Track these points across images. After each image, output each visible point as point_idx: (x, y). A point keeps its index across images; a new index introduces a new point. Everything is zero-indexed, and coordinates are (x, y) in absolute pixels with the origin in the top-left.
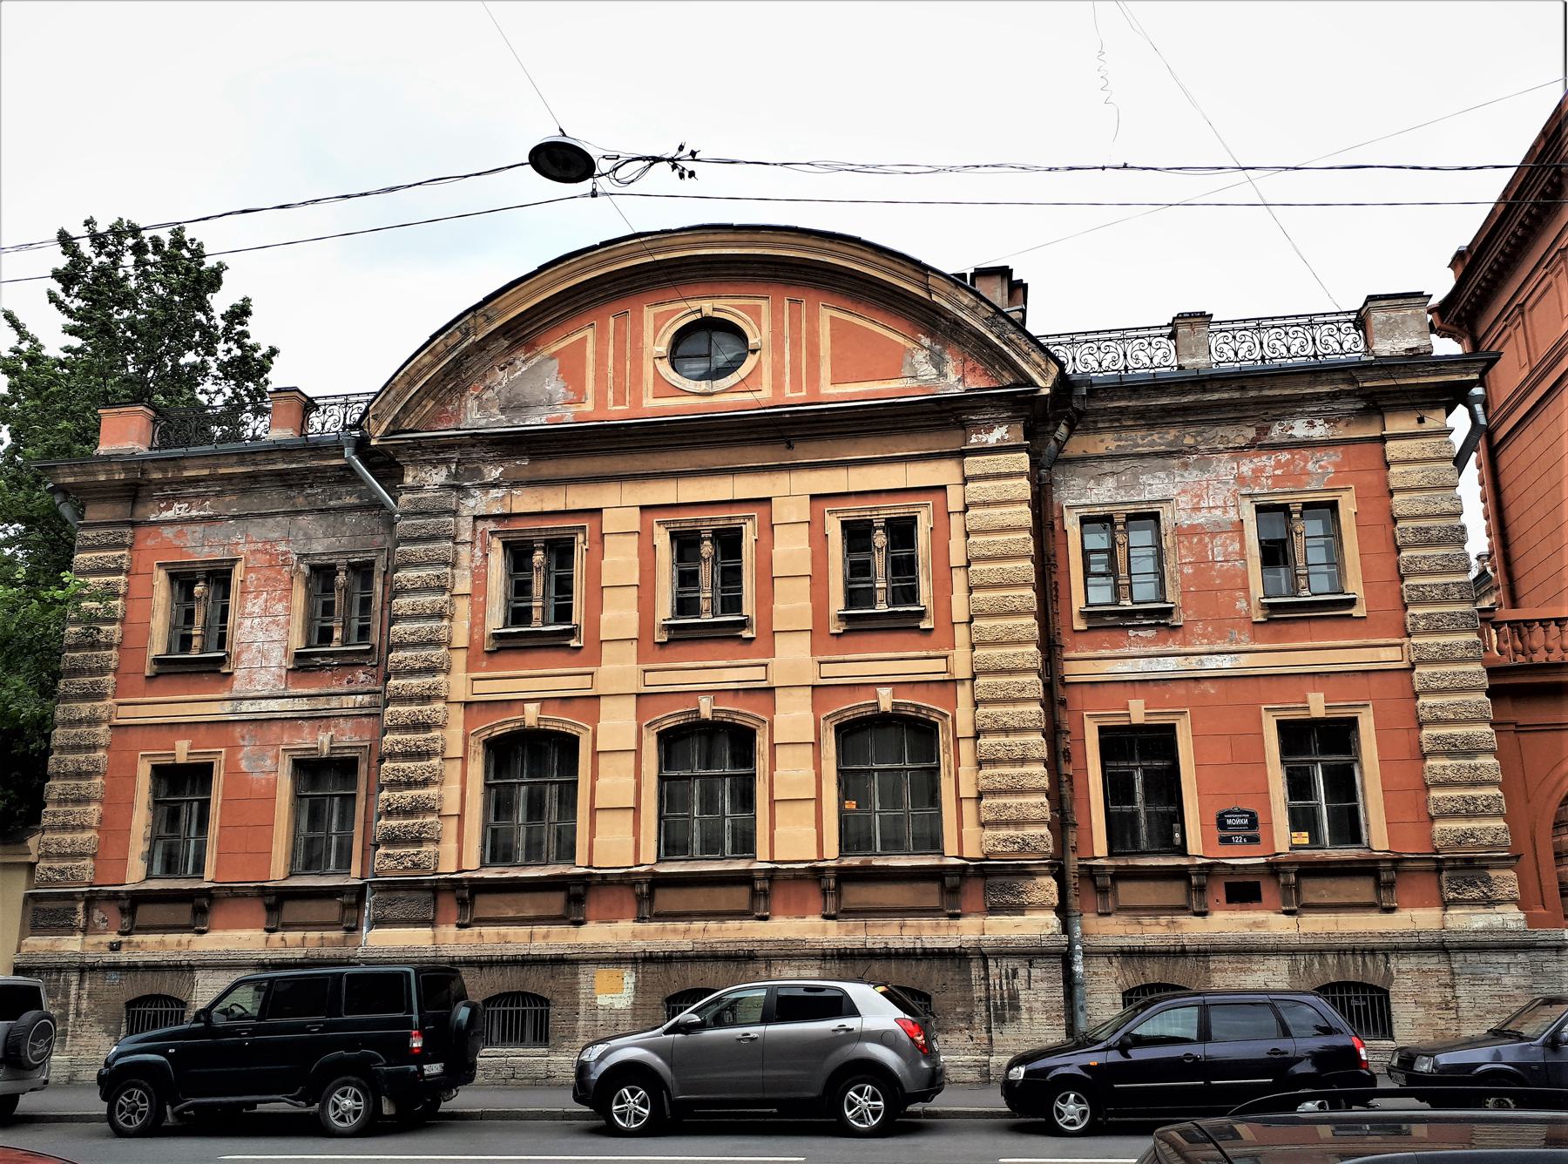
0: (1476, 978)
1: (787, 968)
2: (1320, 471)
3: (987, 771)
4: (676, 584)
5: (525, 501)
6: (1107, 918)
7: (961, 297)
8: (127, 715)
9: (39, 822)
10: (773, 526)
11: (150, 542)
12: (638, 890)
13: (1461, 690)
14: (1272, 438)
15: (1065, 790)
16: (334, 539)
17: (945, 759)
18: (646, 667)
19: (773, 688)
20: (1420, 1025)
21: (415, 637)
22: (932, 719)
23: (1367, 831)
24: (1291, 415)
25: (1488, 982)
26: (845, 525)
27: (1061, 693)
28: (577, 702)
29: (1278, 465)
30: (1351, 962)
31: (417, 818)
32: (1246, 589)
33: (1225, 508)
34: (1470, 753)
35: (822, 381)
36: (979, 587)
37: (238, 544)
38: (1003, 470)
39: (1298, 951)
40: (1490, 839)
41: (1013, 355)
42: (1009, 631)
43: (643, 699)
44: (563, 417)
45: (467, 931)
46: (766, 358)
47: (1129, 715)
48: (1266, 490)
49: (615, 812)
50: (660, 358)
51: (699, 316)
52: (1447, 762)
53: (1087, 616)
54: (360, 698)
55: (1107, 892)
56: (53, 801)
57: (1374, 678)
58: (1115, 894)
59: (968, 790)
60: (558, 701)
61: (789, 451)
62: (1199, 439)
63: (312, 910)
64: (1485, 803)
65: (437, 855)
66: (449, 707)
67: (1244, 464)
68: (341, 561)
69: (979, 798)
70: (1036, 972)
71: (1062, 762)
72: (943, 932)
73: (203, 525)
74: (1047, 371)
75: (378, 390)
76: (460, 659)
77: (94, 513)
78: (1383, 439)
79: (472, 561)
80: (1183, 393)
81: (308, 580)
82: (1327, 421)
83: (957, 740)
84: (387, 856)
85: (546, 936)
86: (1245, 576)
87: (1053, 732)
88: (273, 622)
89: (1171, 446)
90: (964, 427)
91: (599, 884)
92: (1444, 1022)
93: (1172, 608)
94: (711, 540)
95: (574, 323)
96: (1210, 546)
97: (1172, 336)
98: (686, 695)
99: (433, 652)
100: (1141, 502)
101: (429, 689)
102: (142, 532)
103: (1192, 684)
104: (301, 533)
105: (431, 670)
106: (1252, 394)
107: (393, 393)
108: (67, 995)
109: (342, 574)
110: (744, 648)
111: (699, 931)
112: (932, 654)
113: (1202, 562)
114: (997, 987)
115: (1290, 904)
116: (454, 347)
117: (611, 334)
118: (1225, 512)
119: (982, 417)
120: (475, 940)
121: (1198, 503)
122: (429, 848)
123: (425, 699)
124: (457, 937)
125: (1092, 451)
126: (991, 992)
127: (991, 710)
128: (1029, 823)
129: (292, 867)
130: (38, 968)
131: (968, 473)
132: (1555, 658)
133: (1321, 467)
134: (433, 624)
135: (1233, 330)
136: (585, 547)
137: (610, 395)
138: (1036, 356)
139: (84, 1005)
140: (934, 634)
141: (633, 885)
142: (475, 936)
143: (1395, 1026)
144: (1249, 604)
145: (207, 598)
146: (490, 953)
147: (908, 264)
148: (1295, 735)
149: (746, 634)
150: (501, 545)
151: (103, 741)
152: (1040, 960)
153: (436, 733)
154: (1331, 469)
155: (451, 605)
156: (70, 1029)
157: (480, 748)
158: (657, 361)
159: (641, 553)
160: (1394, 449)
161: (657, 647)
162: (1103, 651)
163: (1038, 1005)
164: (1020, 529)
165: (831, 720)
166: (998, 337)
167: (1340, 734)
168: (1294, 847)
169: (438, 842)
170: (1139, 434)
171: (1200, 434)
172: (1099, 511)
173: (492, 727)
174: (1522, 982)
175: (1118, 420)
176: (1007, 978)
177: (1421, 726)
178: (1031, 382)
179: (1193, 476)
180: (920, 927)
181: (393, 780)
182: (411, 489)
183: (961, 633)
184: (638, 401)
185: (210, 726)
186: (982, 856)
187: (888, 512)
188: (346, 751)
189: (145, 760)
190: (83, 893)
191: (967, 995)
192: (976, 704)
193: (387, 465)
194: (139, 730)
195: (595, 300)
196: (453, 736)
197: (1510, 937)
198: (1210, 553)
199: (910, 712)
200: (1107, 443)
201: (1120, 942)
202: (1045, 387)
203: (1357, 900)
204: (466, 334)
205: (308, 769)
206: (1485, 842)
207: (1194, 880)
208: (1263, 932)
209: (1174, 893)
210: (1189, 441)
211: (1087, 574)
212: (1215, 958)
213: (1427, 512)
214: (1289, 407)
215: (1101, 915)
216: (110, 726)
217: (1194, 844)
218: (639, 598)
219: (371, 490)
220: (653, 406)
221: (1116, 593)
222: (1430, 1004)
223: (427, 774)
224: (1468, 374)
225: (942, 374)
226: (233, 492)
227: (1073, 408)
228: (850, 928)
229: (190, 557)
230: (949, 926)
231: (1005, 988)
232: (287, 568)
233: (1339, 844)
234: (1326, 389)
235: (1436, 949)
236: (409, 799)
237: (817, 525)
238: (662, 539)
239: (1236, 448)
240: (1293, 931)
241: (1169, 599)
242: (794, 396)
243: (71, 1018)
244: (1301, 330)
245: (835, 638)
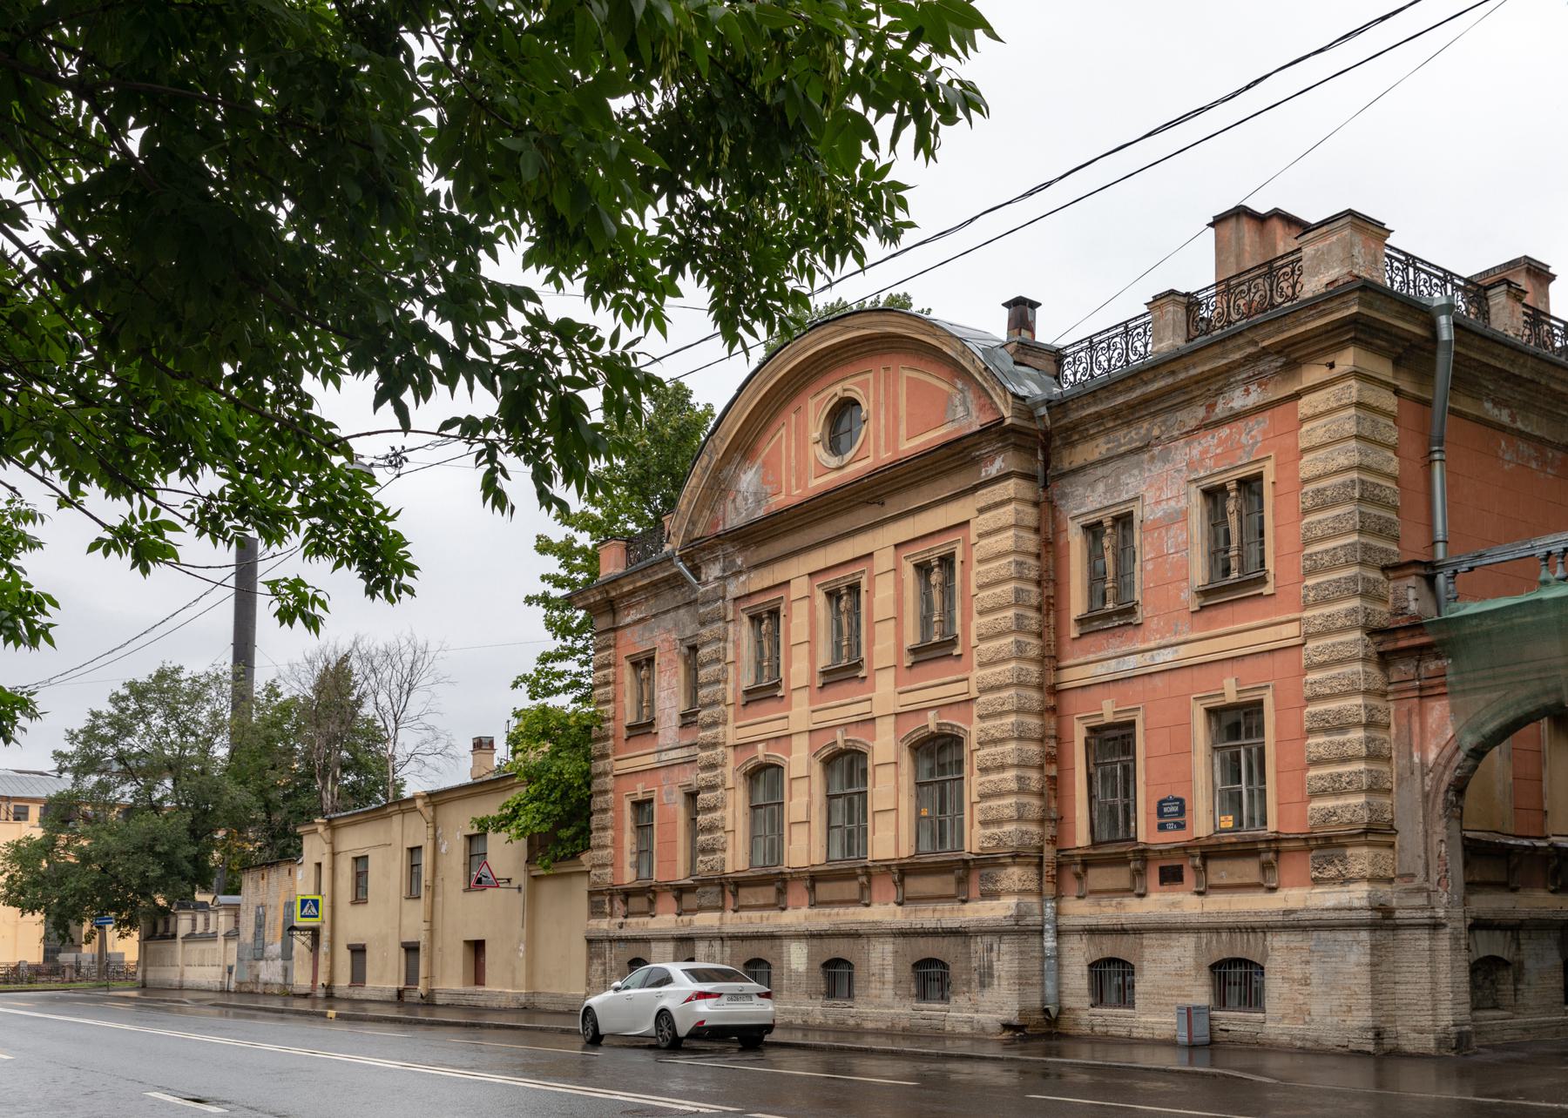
34: (1343, 728)
38: (998, 499)
43: (900, 717)
47: (1223, 694)
51: (836, 399)
57: (1279, 656)
90: (976, 462)
92: (1301, 997)
102: (619, 633)
103: (1146, 679)
106: (1182, 376)
116: (707, 467)
122: (719, 855)
133: (1252, 437)
151: (609, 787)
175: (1102, 424)
179: (1158, 468)
201: (1083, 921)
203: (1247, 880)
208: (1176, 911)
210: (1156, 432)
222: (1294, 980)
224: (1348, 308)
230: (958, 910)
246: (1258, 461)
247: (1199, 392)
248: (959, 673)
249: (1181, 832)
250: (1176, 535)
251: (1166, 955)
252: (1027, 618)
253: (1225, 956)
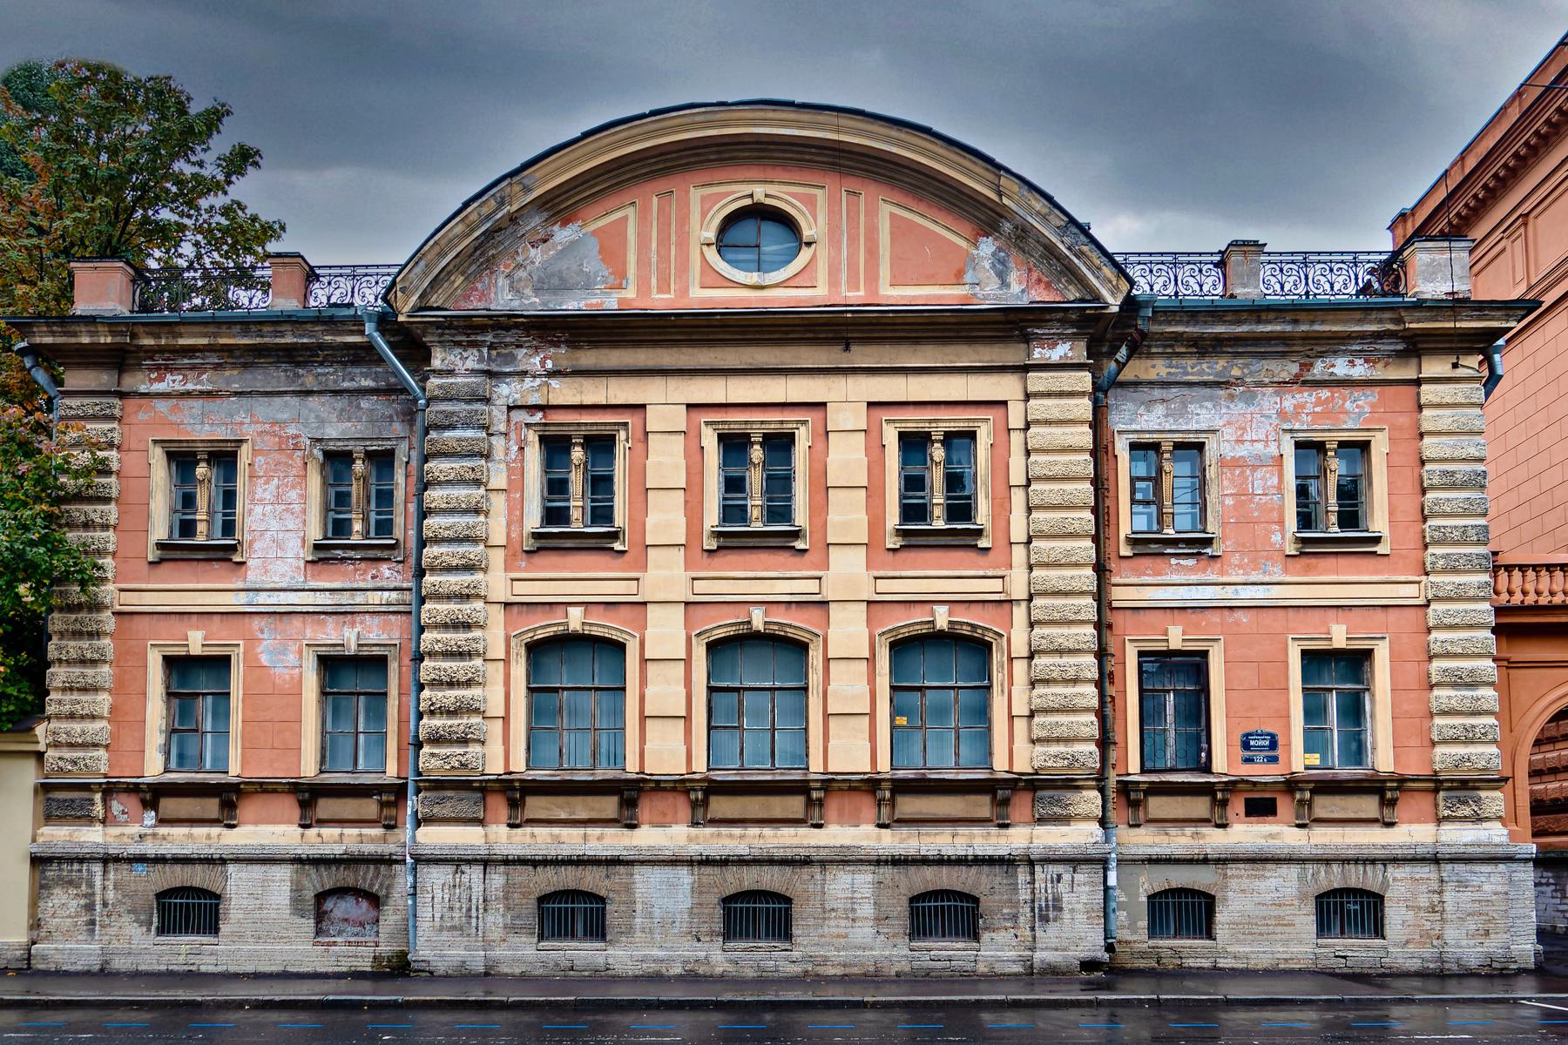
0: (1462, 884)
1: (842, 873)
2: (1357, 410)
3: (1040, 690)
4: (723, 489)
5: (564, 392)
6: (1137, 829)
7: (1033, 203)
8: (133, 601)
9: (43, 710)
10: (647, 433)
11: (142, 416)
12: (693, 796)
13: (1471, 627)
14: (1314, 375)
15: (1109, 710)
16: (350, 424)
17: (998, 677)
18: (695, 574)
19: (828, 602)
21: (451, 533)
22: (986, 638)
23: (1372, 753)
24: (1335, 352)
25: (1470, 889)
26: (903, 436)
27: (1110, 617)
28: (622, 608)
29: (1319, 402)
30: (1353, 870)
31: (461, 718)
32: (1281, 522)
33: (1267, 442)
35: (881, 281)
36: (1038, 507)
37: (242, 423)
39: (1309, 860)
40: (1484, 764)
41: (1084, 269)
42: (1068, 553)
44: (602, 303)
45: (519, 831)
46: (822, 252)
48: (1308, 425)
49: (665, 720)
50: (708, 245)
51: (748, 202)
52: (1452, 693)
53: (1133, 542)
54: (386, 594)
55: (1139, 805)
56: (57, 689)
57: (1392, 613)
58: (1146, 808)
59: (1020, 708)
60: (602, 607)
61: (846, 354)
62: (1246, 371)
63: (348, 807)
64: (1483, 731)
65: (484, 756)
66: (488, 607)
68: (358, 448)
69: (1031, 716)
70: (1079, 877)
71: (1107, 684)
72: (993, 840)
73: (201, 401)
74: (1117, 287)
75: (403, 262)
76: (497, 558)
77: (75, 379)
78: (1418, 382)
79: (507, 454)
80: (1239, 322)
81: (323, 466)
82: (1366, 361)
83: (1011, 659)
84: (433, 755)
85: (599, 838)
86: (1281, 509)
87: (1101, 654)
88: (287, 510)
89: (1220, 377)
91: (652, 790)
93: (1212, 538)
94: (761, 444)
95: (611, 202)
97: (1221, 264)
98: (736, 605)
99: (471, 549)
100: (1189, 432)
101: (467, 587)
103: (1226, 612)
104: (313, 415)
105: (469, 568)
106: (1304, 328)
107: (422, 264)
108: (91, 885)
109: (359, 462)
110: (797, 560)
111: (755, 837)
112: (990, 573)
113: (1243, 495)
114: (1043, 891)
115: (1303, 818)
116: (488, 217)
117: (655, 215)
118: (1266, 446)
119: (1047, 331)
120: (528, 840)
121: (1242, 435)
122: (474, 749)
123: (464, 597)
124: (509, 837)
125: (1144, 377)
126: (1037, 896)
127: (1046, 631)
128: (1078, 740)
129: (321, 765)
130: (58, 858)
131: (1031, 389)
132: (1558, 599)
133: (1358, 406)
134: (469, 519)
135: (1200, 263)
136: (627, 446)
137: (654, 281)
138: (1108, 271)
139: (111, 895)
140: (991, 553)
141: (687, 792)
142: (528, 836)
143: (1387, 927)
144: (1283, 538)
145: (209, 481)
146: (544, 852)
147: (980, 162)
148: (1314, 660)
149: (799, 545)
150: (537, 438)
152: (1084, 867)
153: (477, 633)
154: (1367, 409)
155: (488, 500)
156: (98, 919)
157: (523, 651)
158: (705, 248)
159: (687, 455)
160: (1428, 392)
161: (706, 554)
162: (1147, 578)
163: (1080, 906)
164: (1080, 450)
165: (886, 636)
166: (1069, 249)
167: (1356, 661)
168: (1307, 768)
169: (483, 743)
170: (1190, 362)
171: (1246, 366)
172: (1147, 438)
173: (535, 629)
174: (1499, 888)
175: (1172, 346)
176: (1052, 882)
177: (1431, 658)
178: (1097, 298)
179: (1239, 408)
180: (972, 836)
181: (434, 680)
182: (439, 373)
183: (1019, 553)
184: (685, 291)
185: (225, 616)
186: (1031, 771)
187: (948, 425)
188: (374, 649)
189: (156, 649)
190: (100, 784)
191: (1013, 897)
192: (1032, 625)
193: (413, 347)
194: (147, 618)
195: (637, 176)
196: (495, 635)
197: (1493, 850)
198: (1250, 486)
199: (966, 631)
200: (1158, 369)
201: (1150, 851)
202: (1114, 303)
203: (1363, 816)
204: (502, 203)
205: (332, 665)
206: (1480, 766)
207: (1219, 795)
208: (1277, 842)
209: (1199, 806)
210: (1236, 372)
211: (1133, 501)
212: (1234, 866)
213: (1454, 456)
214: (1333, 344)
215: (1131, 826)
216: (113, 613)
217: (1220, 763)
218: (686, 502)
219: (396, 373)
220: (700, 296)
221: (1160, 522)
222: (1419, 908)
223: (470, 675)
224: (1507, 321)
225: (1005, 284)
226: (234, 366)
227: (1137, 329)
228: (904, 836)
229: (188, 433)
230: (999, 836)
231: (1049, 891)
232: (299, 453)
233: (1347, 765)
234: (1374, 328)
235: (1429, 860)
236: (453, 700)
237: (874, 434)
238: (710, 441)
239: (1279, 383)
240: (1304, 842)
241: (1210, 528)
242: (853, 295)
243: (98, 908)
244: (1165, 268)
245: (891, 553)
246: (1368, 430)
247: (1301, 349)
248: (982, 568)
249: (1272, 766)
250: (1261, 481)
251: (1262, 885)
253: (1336, 886)
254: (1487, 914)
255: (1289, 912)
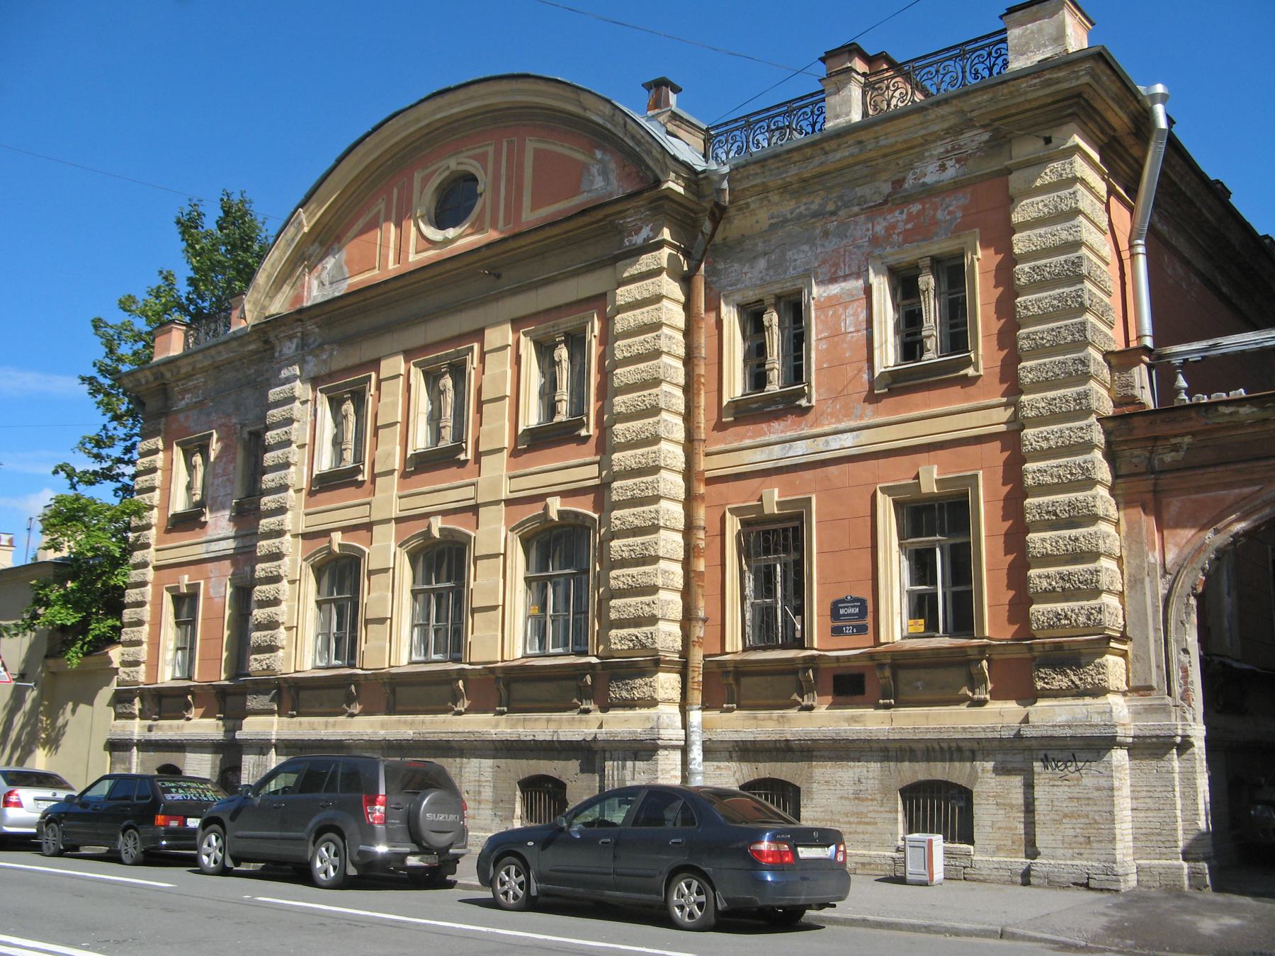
2: (948, 217)
14: (906, 190)
20: (999, 828)
67: (878, 223)
96: (843, 317)
116: (293, 239)
133: (950, 213)
168: (411, 663)
208: (857, 727)
248: (584, 456)
252: (674, 396)
254: (1087, 816)
255: (871, 808)
